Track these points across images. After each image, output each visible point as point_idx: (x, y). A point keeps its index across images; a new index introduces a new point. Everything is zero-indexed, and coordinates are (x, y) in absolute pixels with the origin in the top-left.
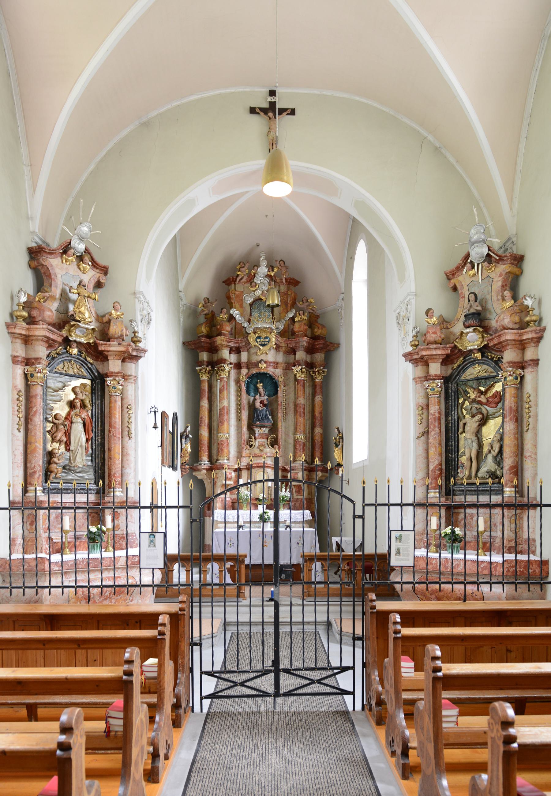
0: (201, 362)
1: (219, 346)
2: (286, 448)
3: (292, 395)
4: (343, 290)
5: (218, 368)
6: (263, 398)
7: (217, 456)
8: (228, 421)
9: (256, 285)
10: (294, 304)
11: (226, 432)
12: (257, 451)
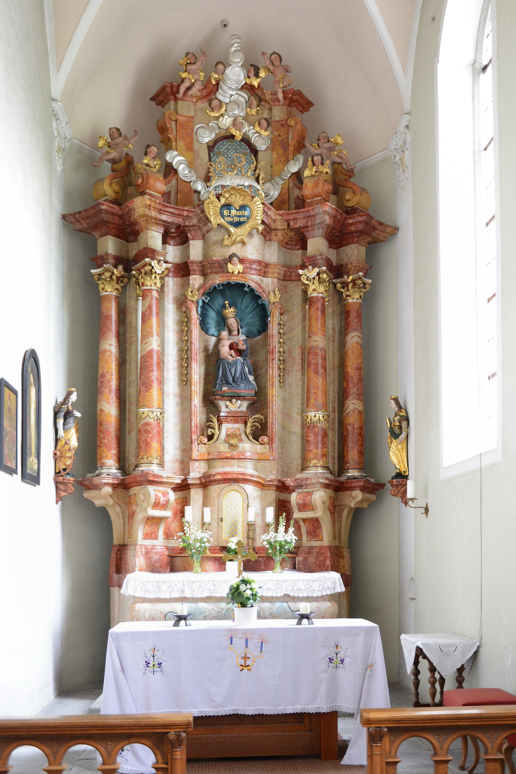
0: (102, 257)
1: (142, 222)
2: (284, 443)
3: (297, 334)
4: (407, 107)
5: (139, 270)
6: (235, 339)
7: (137, 457)
8: (161, 381)
9: (221, 107)
10: (300, 147)
11: (156, 405)
12: (223, 448)
